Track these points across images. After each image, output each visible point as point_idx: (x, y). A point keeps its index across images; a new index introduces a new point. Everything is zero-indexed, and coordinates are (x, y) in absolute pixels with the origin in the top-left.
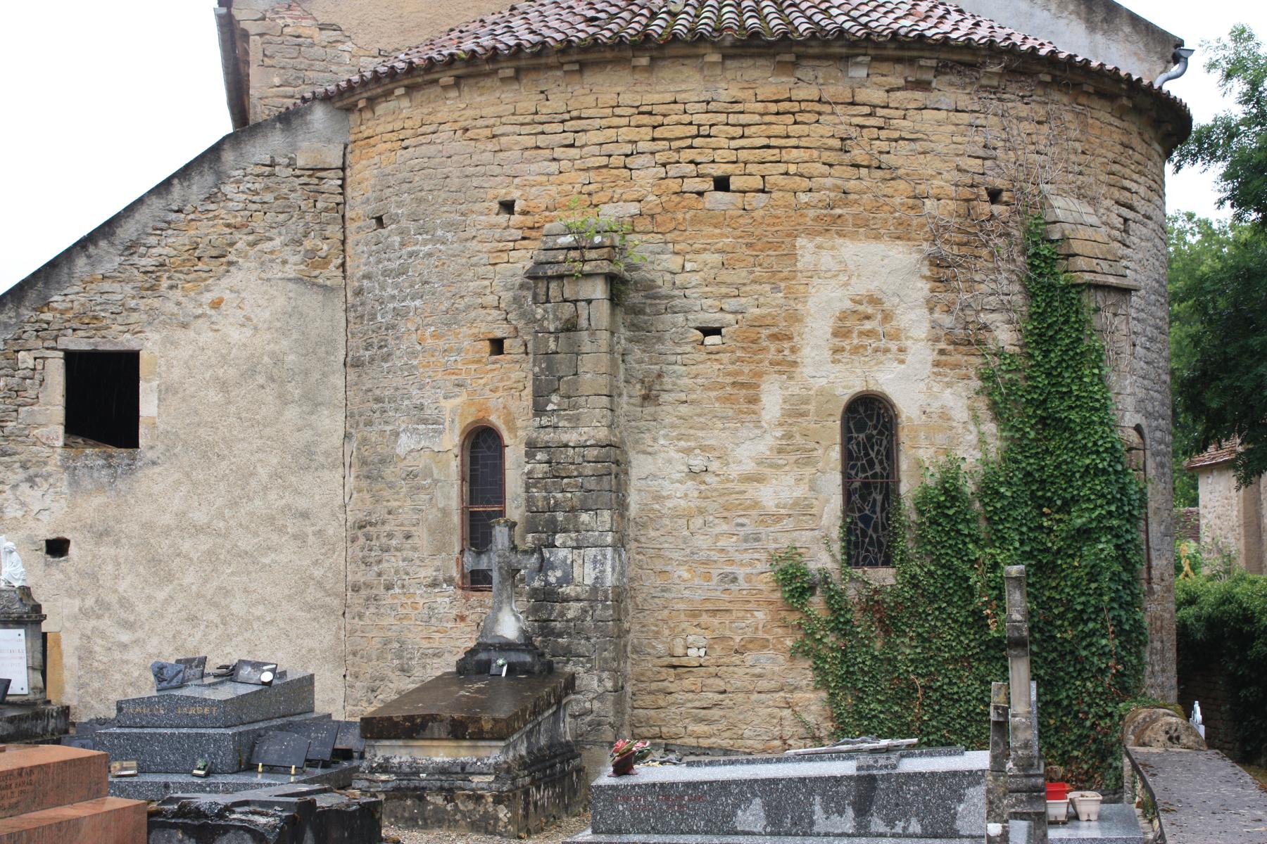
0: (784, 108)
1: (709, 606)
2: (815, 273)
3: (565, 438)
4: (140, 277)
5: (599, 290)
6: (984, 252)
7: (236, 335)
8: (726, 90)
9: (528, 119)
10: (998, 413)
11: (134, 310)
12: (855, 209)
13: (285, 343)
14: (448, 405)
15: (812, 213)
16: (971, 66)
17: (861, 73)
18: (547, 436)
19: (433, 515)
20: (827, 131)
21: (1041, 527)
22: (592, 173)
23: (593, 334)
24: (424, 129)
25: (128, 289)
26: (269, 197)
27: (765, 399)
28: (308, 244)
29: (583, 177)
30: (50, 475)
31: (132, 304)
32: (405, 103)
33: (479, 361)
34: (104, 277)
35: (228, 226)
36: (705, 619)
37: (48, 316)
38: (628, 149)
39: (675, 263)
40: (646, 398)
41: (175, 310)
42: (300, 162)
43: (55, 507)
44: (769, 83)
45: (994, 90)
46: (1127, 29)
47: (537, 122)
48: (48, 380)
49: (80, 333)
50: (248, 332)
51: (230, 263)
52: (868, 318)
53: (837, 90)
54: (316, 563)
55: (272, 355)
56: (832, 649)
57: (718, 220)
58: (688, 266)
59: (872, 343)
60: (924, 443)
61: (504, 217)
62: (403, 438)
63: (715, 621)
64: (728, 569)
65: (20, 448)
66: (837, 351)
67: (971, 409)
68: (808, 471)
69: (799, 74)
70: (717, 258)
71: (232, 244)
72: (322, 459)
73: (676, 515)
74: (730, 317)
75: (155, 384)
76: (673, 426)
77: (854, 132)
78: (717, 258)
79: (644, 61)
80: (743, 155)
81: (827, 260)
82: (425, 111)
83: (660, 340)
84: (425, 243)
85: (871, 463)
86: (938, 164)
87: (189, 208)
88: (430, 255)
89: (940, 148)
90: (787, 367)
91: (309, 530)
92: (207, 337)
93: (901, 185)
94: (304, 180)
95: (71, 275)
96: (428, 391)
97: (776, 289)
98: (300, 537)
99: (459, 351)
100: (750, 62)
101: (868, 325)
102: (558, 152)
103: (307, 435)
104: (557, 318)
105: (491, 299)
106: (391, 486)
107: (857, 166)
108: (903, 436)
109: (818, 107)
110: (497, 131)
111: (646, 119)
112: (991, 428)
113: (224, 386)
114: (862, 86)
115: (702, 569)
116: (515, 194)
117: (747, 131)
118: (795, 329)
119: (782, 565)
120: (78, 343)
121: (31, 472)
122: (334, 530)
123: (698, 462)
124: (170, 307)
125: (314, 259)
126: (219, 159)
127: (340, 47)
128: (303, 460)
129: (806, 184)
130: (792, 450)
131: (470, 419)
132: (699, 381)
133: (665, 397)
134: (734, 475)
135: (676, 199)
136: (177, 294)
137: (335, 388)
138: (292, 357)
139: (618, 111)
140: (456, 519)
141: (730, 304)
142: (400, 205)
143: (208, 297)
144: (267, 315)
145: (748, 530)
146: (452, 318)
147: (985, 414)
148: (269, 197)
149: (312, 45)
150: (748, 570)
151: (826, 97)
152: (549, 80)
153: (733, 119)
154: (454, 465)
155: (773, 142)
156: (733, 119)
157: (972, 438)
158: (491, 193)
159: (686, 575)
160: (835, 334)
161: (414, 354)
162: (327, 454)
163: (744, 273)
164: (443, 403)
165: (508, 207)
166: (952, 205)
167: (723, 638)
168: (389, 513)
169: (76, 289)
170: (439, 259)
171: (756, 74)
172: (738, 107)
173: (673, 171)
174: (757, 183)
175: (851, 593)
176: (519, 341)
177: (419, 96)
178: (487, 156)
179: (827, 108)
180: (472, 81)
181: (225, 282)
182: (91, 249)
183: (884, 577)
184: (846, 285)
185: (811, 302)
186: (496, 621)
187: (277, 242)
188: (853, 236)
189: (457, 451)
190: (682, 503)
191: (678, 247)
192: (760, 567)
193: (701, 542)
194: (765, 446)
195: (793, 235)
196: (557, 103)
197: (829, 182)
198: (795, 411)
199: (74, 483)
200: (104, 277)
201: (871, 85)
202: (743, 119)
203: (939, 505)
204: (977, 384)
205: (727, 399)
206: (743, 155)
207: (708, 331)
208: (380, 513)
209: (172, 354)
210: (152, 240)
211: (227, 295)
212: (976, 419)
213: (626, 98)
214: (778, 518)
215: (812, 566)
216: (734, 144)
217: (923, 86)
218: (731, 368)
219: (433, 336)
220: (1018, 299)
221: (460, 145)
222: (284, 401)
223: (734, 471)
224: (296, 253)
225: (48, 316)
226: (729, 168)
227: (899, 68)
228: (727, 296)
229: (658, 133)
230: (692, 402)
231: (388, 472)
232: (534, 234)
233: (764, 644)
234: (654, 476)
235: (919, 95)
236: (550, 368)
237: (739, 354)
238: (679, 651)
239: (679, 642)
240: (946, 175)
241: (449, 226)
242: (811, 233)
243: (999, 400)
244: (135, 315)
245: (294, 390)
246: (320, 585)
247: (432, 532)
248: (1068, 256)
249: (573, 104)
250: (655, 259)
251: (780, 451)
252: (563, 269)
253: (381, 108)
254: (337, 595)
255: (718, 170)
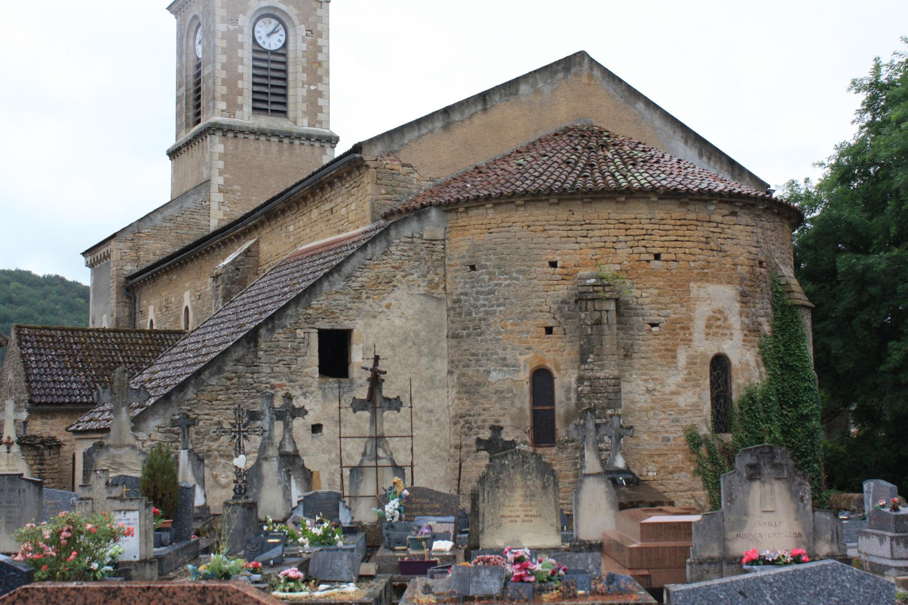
0: (682, 223)
1: (658, 452)
2: (698, 299)
3: (598, 374)
4: (353, 292)
5: (612, 306)
6: (758, 290)
7: (398, 322)
8: (659, 214)
9: (564, 223)
10: (766, 364)
11: (351, 309)
12: (712, 270)
13: (420, 326)
14: (522, 358)
15: (696, 271)
16: (752, 205)
17: (712, 208)
18: (589, 374)
19: (514, 411)
20: (700, 234)
21: (782, 414)
22: (597, 250)
23: (609, 326)
24: (503, 225)
25: (347, 298)
26: (411, 253)
27: (679, 356)
28: (429, 277)
29: (593, 252)
30: (313, 392)
31: (349, 305)
32: (491, 211)
33: (539, 337)
34: (337, 292)
35: (393, 267)
36: (656, 458)
37: (310, 311)
38: (615, 239)
39: (637, 293)
40: (626, 356)
41: (370, 309)
42: (425, 237)
43: (316, 408)
44: (677, 212)
45: (758, 216)
46: (748, 179)
47: (568, 225)
48: (311, 344)
49: (326, 320)
50: (404, 321)
51: (394, 286)
52: (719, 319)
53: (703, 215)
54: (436, 435)
55: (414, 332)
56: (710, 471)
57: (654, 273)
58: (644, 295)
59: (721, 331)
60: (740, 376)
61: (551, 270)
62: (493, 374)
63: (661, 459)
64: (666, 435)
65: (299, 378)
66: (708, 334)
67: (757, 361)
68: (698, 390)
69: (688, 207)
70: (656, 291)
71: (395, 277)
72: (438, 383)
73: (641, 410)
74: (663, 319)
75: (361, 346)
76: (639, 369)
77: (711, 235)
78: (656, 291)
79: (623, 199)
80: (667, 244)
81: (702, 293)
82: (504, 215)
83: (632, 329)
84: (505, 279)
85: (719, 386)
86: (741, 250)
87: (375, 258)
88: (509, 285)
89: (742, 242)
90: (688, 342)
91: (433, 419)
92: (384, 323)
93: (729, 259)
94: (426, 245)
95: (321, 291)
96: (509, 351)
97: (682, 306)
98: (429, 422)
99: (528, 332)
100: (668, 201)
101: (719, 323)
102: (579, 239)
103: (431, 372)
104: (591, 318)
105: (545, 308)
106: (485, 397)
107: (712, 250)
108: (733, 374)
109: (696, 223)
110: (546, 228)
111: (622, 226)
112: (763, 369)
113: (393, 347)
114: (713, 214)
115: (654, 435)
116: (558, 258)
117: (668, 233)
118: (691, 324)
119: (688, 433)
120: (325, 325)
121: (304, 390)
122: (445, 419)
123: (651, 386)
124: (367, 307)
125: (432, 284)
126: (388, 234)
127: (412, 175)
128: (429, 384)
129: (693, 258)
130: (691, 380)
131: (535, 365)
132: (651, 348)
133: (634, 355)
134: (667, 392)
135: (637, 263)
136: (370, 301)
137: (443, 348)
138: (423, 333)
139: (609, 221)
140: (528, 413)
141: (662, 313)
142: (487, 260)
143: (385, 303)
144: (411, 312)
145: (673, 417)
146: (523, 317)
147: (761, 363)
148: (411, 253)
149: (399, 174)
150: (674, 435)
151: (700, 218)
152: (576, 206)
153: (662, 227)
154: (527, 387)
155: (679, 238)
156: (662, 227)
157: (757, 374)
158: (544, 257)
159: (647, 438)
160: (707, 327)
161: (499, 333)
162: (440, 381)
163: (668, 299)
164: (519, 357)
165: (553, 264)
166: (747, 269)
167: (664, 467)
168: (484, 410)
169: (323, 298)
170: (515, 287)
171: (670, 207)
172: (664, 222)
173: (636, 250)
174: (673, 257)
175: (717, 445)
176: (561, 328)
177: (500, 208)
178: (541, 240)
179: (700, 224)
180: (532, 203)
181: (392, 295)
182: (331, 278)
183: (728, 437)
184: (710, 304)
185: (697, 311)
186: (614, 460)
187: (415, 276)
188: (711, 282)
189: (528, 380)
190: (644, 405)
191: (639, 286)
192: (679, 434)
193: (653, 422)
194: (679, 378)
195: (688, 281)
196: (578, 216)
197: (702, 257)
198: (691, 362)
199: (325, 396)
200: (337, 292)
201: (718, 213)
202: (666, 227)
203: (750, 405)
204: (758, 350)
205: (662, 357)
206: (667, 244)
207: (653, 325)
208: (477, 409)
209: (369, 331)
210: (358, 274)
211: (393, 302)
212: (758, 365)
213: (613, 216)
214: (686, 411)
215: (701, 433)
216: (662, 239)
217: (734, 214)
218: (664, 342)
219: (512, 324)
220: (770, 311)
221: (525, 233)
222: (420, 354)
223: (667, 390)
224: (424, 281)
225: (310, 311)
226: (661, 250)
227: (727, 206)
228: (661, 309)
229: (628, 232)
230: (647, 358)
231: (482, 390)
232: (568, 277)
233: (682, 469)
234: (631, 392)
235: (734, 218)
236: (589, 342)
237: (667, 336)
238: (645, 473)
239: (645, 469)
240: (745, 255)
241: (520, 272)
242: (695, 281)
243: (766, 359)
244: (351, 311)
245: (425, 349)
246: (438, 445)
247: (513, 419)
248: (789, 292)
249: (586, 217)
250: (633, 293)
251: (686, 380)
252: (595, 296)
253: (473, 213)
254: (446, 451)
255: (656, 251)
